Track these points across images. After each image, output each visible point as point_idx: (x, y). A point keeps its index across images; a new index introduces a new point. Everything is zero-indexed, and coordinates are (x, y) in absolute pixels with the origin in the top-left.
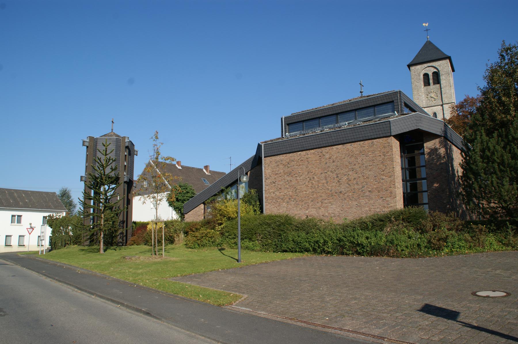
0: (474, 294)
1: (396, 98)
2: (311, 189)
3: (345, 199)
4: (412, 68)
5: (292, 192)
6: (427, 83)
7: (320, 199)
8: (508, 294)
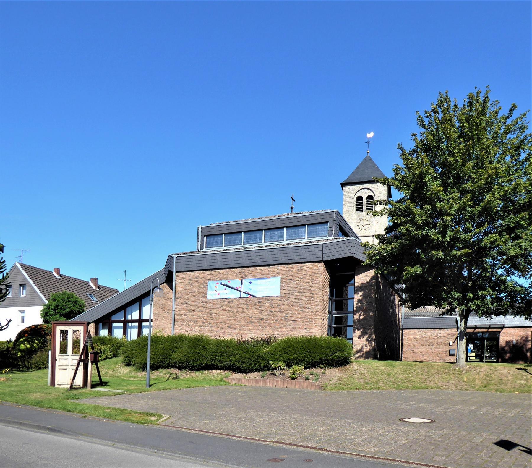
0: (402, 420)
1: (331, 219)
2: (229, 313)
3: (266, 327)
4: (346, 188)
5: (207, 315)
6: (359, 208)
7: (238, 325)
8: (432, 421)
